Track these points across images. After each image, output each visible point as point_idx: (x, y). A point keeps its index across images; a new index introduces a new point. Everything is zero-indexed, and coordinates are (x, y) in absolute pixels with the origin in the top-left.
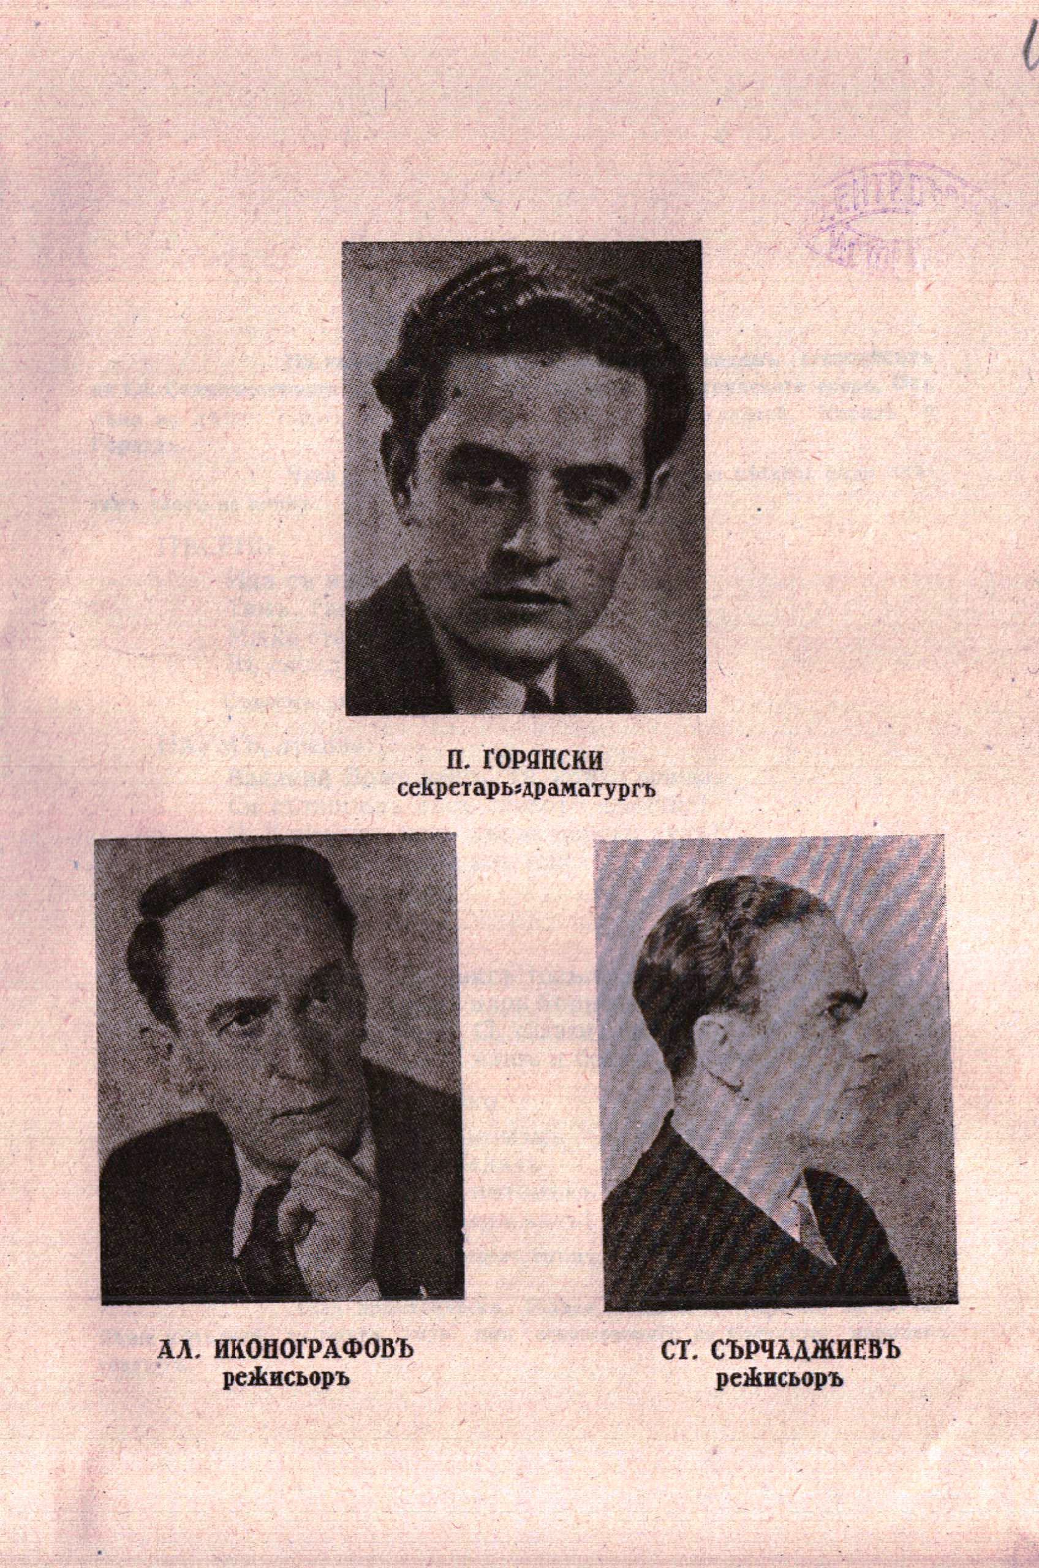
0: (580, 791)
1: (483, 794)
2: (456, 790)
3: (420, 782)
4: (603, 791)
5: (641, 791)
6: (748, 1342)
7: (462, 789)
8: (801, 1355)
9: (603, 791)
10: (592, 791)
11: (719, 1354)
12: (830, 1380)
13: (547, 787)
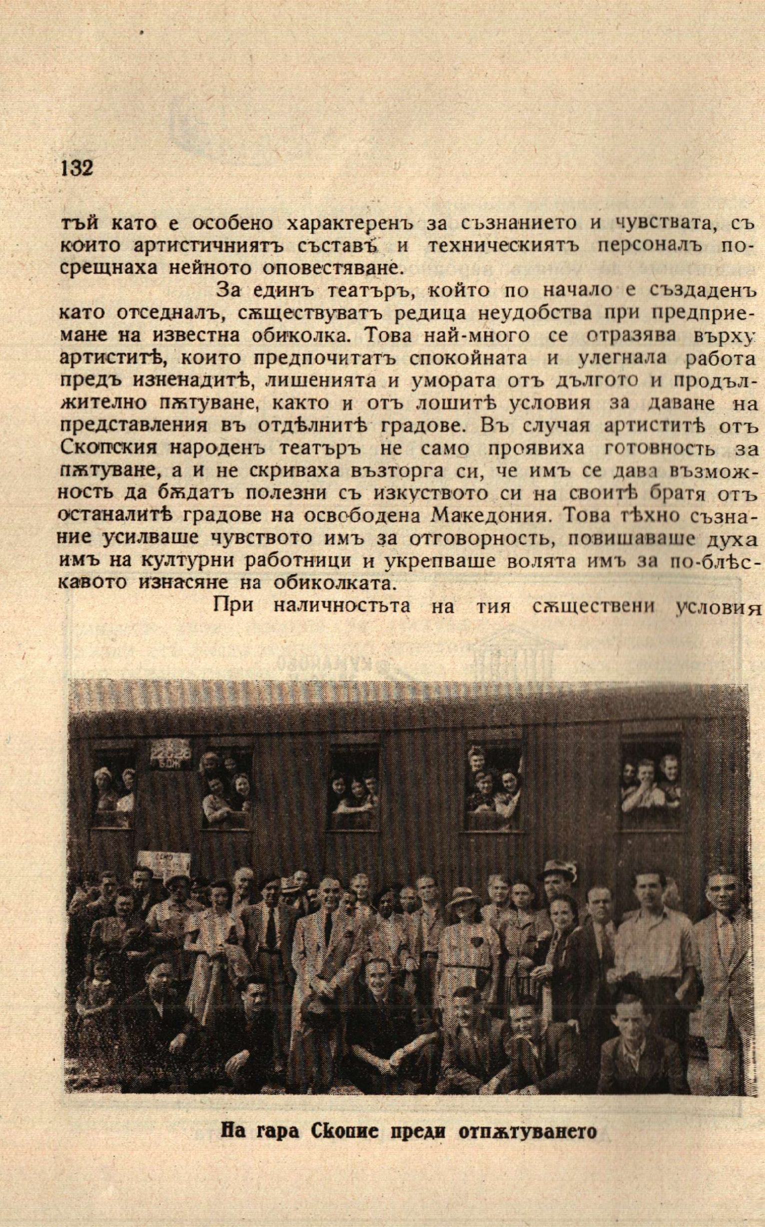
1: (273, 1136)
2: (573, 1134)
4: (520, 1133)
7: (578, 1133)
9: (520, 1133)
11: (317, 1133)
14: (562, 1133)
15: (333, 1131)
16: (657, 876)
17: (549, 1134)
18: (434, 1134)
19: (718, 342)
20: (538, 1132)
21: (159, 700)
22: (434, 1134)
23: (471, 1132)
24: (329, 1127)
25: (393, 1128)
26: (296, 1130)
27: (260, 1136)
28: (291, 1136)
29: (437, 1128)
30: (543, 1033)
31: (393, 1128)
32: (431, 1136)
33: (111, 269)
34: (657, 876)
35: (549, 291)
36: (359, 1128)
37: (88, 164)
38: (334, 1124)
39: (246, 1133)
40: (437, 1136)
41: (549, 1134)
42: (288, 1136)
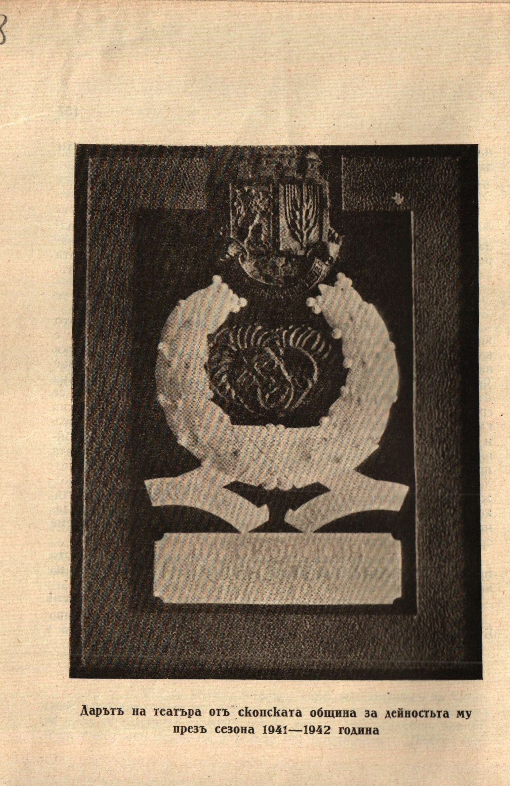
0: (141, 713)
3: (244, 709)
5: (222, 713)
6: (189, 710)
8: (84, 713)
10: (174, 712)
12: (103, 712)
13: (195, 711)
14: (415, 714)
15: (251, 713)
16: (168, 588)
17: (408, 714)
18: (357, 732)
19: (188, 715)
21: (237, 500)
22: (357, 732)
23: (216, 712)
24: (248, 710)
25: (175, 727)
26: (447, 713)
27: (341, 733)
28: (196, 715)
29: (359, 729)
30: (275, 367)
31: (175, 727)
32: (355, 733)
33: (335, 714)
34: (168, 588)
35: (313, 714)
36: (337, 711)
37: (327, 728)
38: (252, 708)
39: (380, 732)
40: (359, 733)
41: (408, 714)
42: (194, 715)
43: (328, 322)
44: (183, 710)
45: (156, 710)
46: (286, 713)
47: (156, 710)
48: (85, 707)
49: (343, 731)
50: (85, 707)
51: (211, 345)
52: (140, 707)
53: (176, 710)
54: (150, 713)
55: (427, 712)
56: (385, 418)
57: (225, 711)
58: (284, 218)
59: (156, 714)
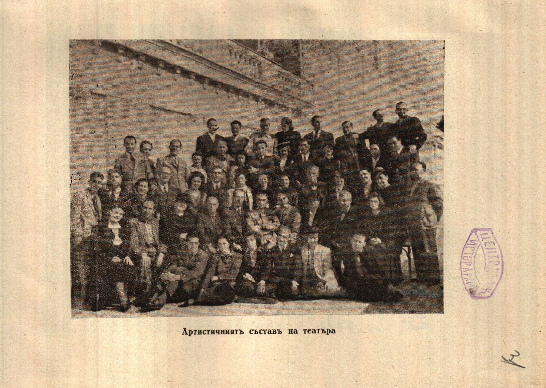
5: (239, 332)
20: (227, 332)
23: (194, 332)
43: (257, 300)
44: (255, 331)
45: (305, 330)
46: (315, 331)
47: (305, 330)
48: (185, 330)
49: (306, 331)
50: (185, 330)
51: (130, 249)
52: (292, 336)
53: (318, 330)
54: (301, 332)
55: (208, 331)
56: (412, 116)
57: (241, 331)
58: (135, 232)
59: (305, 333)
